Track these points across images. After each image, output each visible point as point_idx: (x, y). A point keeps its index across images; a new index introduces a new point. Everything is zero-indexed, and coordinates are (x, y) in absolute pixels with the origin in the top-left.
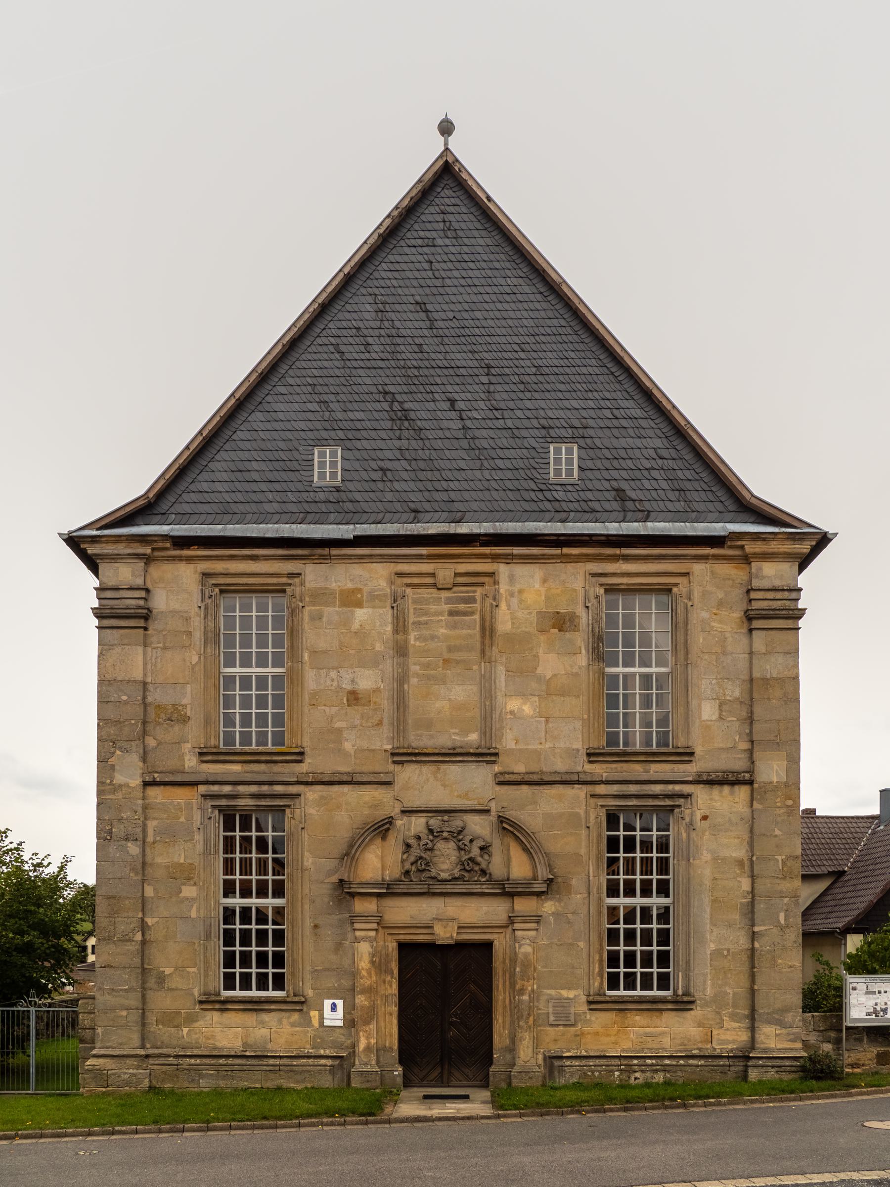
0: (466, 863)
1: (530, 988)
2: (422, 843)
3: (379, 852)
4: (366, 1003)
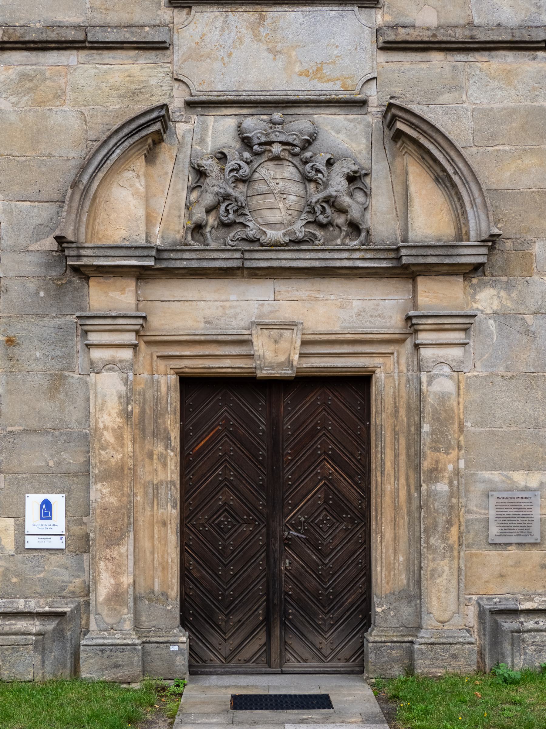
0: (318, 209)
1: (450, 467)
2: (229, 166)
3: (140, 185)
4: (113, 500)
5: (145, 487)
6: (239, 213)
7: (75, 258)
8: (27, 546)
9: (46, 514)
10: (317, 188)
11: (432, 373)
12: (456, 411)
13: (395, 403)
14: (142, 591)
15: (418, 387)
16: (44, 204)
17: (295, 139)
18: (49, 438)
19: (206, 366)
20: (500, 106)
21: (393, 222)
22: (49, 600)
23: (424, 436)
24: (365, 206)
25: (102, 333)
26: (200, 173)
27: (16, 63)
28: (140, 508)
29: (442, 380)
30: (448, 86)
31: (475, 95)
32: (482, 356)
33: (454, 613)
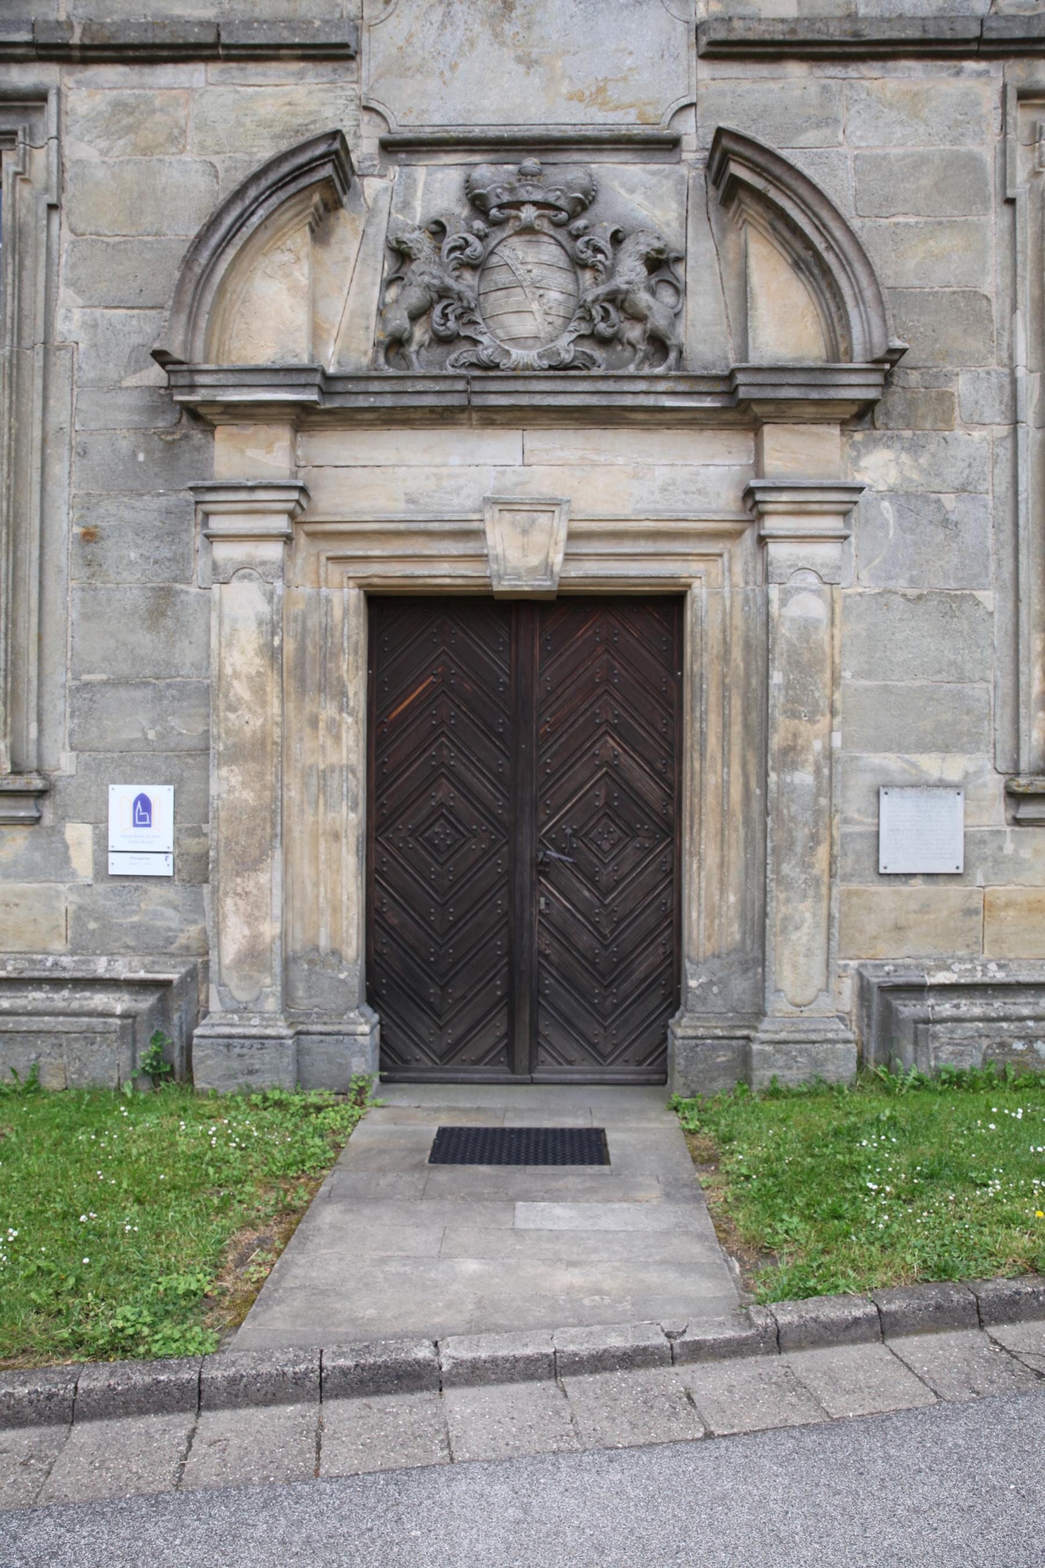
0: (597, 312)
1: (817, 745)
2: (449, 242)
3: (302, 274)
4: (248, 796)
5: (306, 773)
6: (465, 320)
7: (187, 390)
8: (112, 871)
9: (142, 818)
10: (595, 279)
11: (787, 586)
12: (827, 650)
13: (724, 638)
14: (298, 947)
15: (763, 610)
16: (148, 312)
17: (559, 198)
18: (149, 692)
19: (408, 573)
20: (900, 151)
21: (722, 339)
22: (148, 960)
23: (773, 691)
24: (676, 310)
25: (233, 517)
26: (401, 254)
27: (106, 85)
28: (295, 810)
29: (804, 596)
30: (813, 119)
31: (858, 133)
32: (870, 560)
33: (820, 990)
